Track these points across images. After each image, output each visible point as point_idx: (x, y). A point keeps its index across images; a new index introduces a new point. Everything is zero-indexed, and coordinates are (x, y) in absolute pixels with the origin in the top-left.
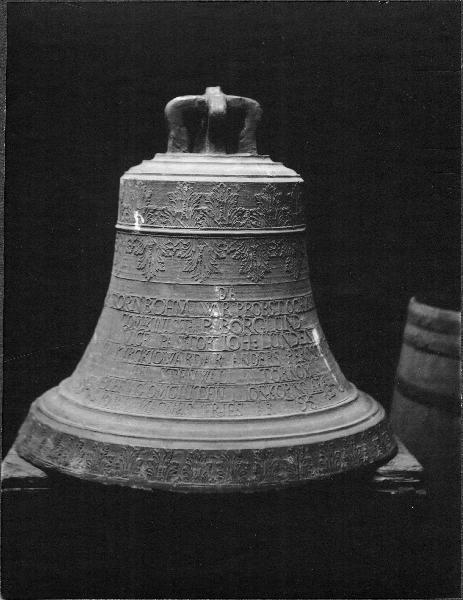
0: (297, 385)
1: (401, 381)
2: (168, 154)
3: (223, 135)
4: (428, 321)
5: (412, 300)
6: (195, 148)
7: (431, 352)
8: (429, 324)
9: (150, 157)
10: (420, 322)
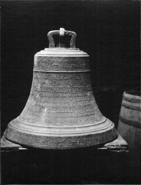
0: (89, 116)
1: (121, 118)
2: (49, 48)
3: (63, 42)
4: (129, 99)
5: (124, 92)
6: (57, 46)
7: (130, 108)
8: (130, 100)
9: (43, 49)
10: (127, 99)
